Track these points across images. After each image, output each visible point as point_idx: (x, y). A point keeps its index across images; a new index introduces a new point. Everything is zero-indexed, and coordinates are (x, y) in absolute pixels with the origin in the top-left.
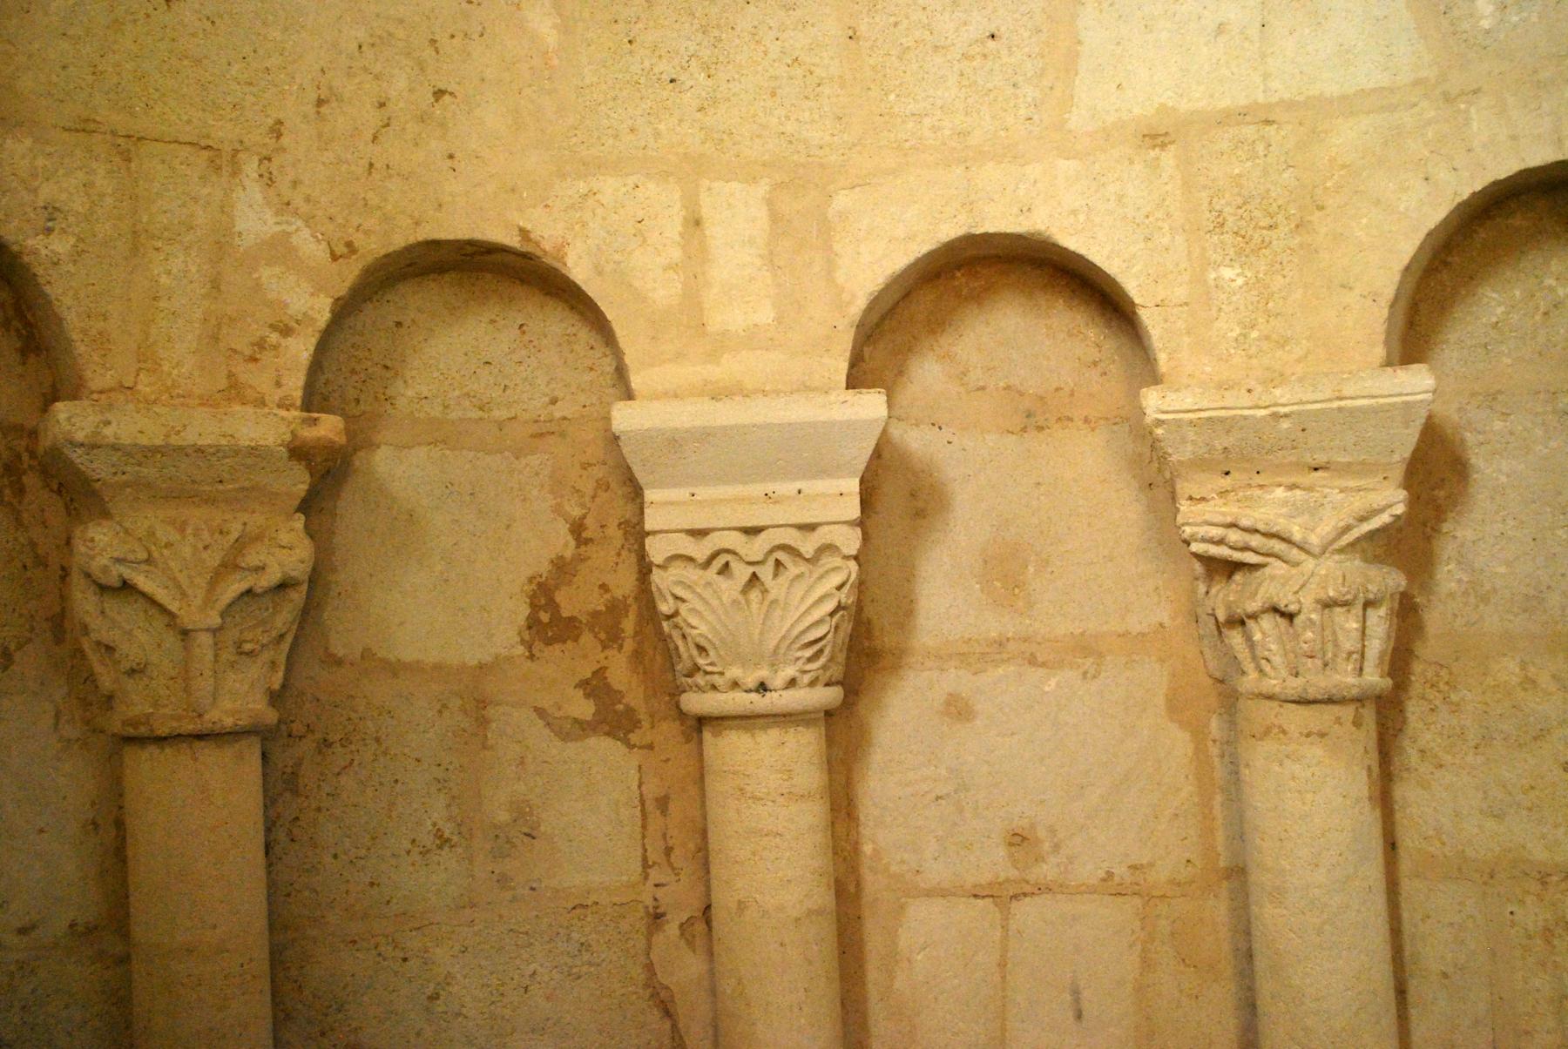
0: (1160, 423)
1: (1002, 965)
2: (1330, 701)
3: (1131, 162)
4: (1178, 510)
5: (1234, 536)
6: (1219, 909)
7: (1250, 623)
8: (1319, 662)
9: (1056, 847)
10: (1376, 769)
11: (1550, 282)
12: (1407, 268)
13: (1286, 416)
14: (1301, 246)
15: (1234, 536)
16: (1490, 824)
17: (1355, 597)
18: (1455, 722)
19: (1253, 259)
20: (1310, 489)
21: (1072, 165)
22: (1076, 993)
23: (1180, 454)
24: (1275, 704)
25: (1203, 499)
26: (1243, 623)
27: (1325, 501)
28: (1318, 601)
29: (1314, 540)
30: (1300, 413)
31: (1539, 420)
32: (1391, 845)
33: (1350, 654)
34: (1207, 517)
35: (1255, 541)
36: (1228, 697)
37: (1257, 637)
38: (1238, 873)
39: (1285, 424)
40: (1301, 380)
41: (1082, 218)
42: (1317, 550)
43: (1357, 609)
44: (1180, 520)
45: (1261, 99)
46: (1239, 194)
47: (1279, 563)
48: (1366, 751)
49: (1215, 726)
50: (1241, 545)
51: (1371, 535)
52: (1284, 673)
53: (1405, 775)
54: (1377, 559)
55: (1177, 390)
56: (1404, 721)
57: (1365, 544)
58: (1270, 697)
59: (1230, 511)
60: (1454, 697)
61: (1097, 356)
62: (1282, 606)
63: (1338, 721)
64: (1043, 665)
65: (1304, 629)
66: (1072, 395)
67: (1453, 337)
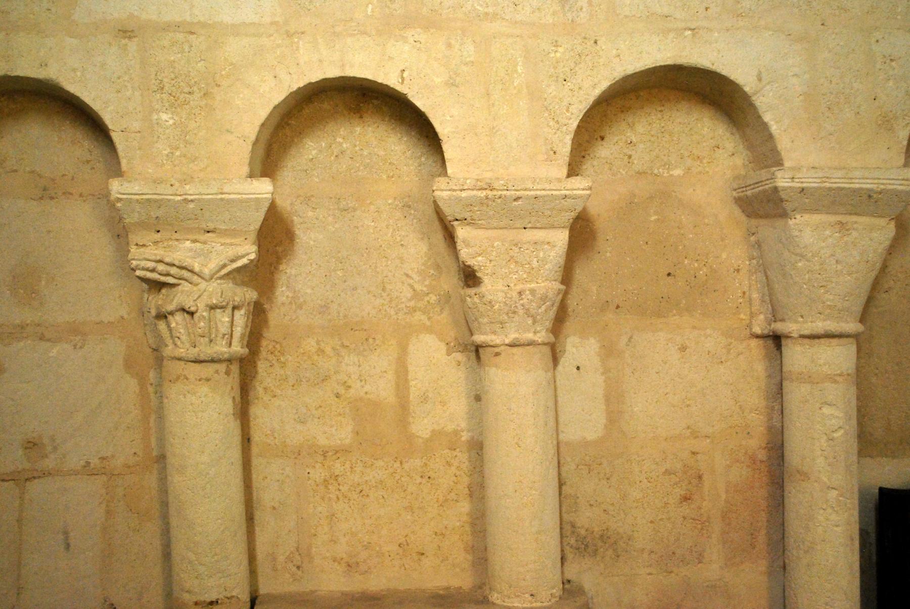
0: (119, 200)
1: (19, 521)
2: (213, 361)
3: (110, 44)
4: (129, 251)
5: (161, 267)
6: (151, 480)
7: (170, 317)
8: (207, 339)
9: (55, 448)
10: (238, 399)
11: (339, 140)
12: (263, 125)
13: (192, 201)
14: (206, 105)
15: (161, 267)
16: (299, 427)
17: (228, 304)
18: (282, 372)
19: (179, 110)
20: (205, 243)
21: (74, 41)
22: (66, 533)
23: (130, 219)
24: (182, 363)
25: (144, 245)
26: (166, 317)
27: (213, 250)
28: (207, 306)
29: (206, 272)
30: (199, 200)
31: (331, 213)
32: (246, 440)
33: (224, 335)
34: (147, 256)
35: (173, 271)
36: (158, 358)
37: (173, 325)
38: (162, 458)
39: (191, 206)
40: (201, 181)
41: (79, 74)
42: (207, 277)
43: (229, 310)
44: (130, 257)
45: (188, 19)
46: (173, 72)
47: (186, 284)
48: (232, 388)
49: (152, 375)
50: (165, 272)
51: (238, 270)
52: (188, 345)
53: (256, 401)
54: (244, 284)
55: (130, 182)
56: (256, 372)
57: (235, 274)
58: (180, 359)
59: (159, 253)
60: (282, 359)
61: (89, 157)
62: (187, 307)
63: (217, 372)
64: (49, 340)
65: (199, 321)
66: (73, 179)
67: (290, 164)
